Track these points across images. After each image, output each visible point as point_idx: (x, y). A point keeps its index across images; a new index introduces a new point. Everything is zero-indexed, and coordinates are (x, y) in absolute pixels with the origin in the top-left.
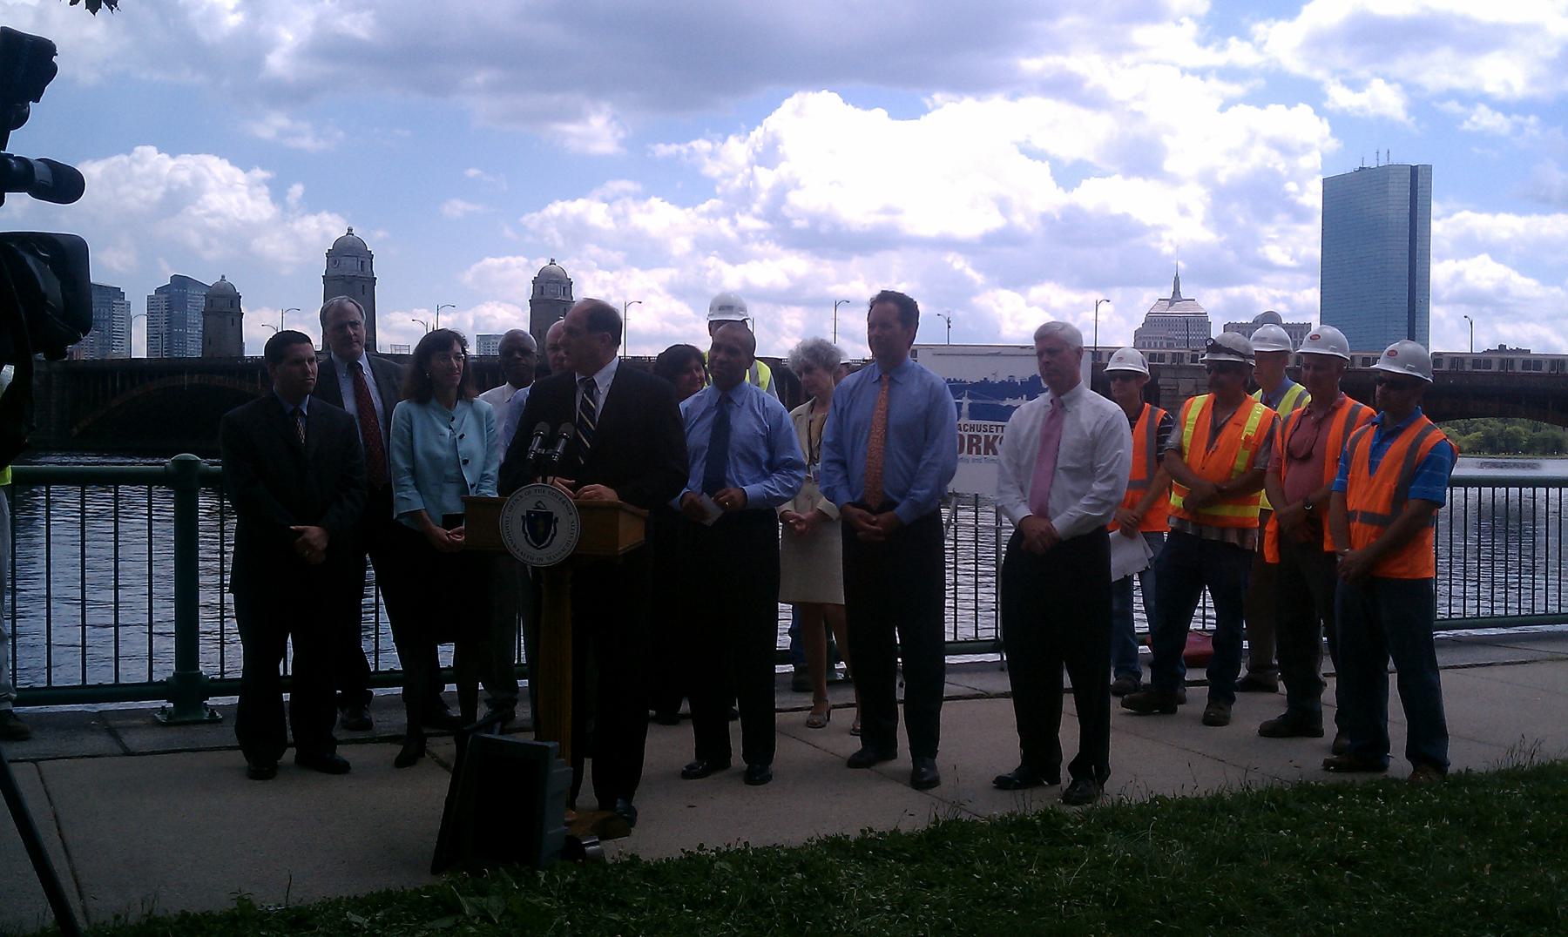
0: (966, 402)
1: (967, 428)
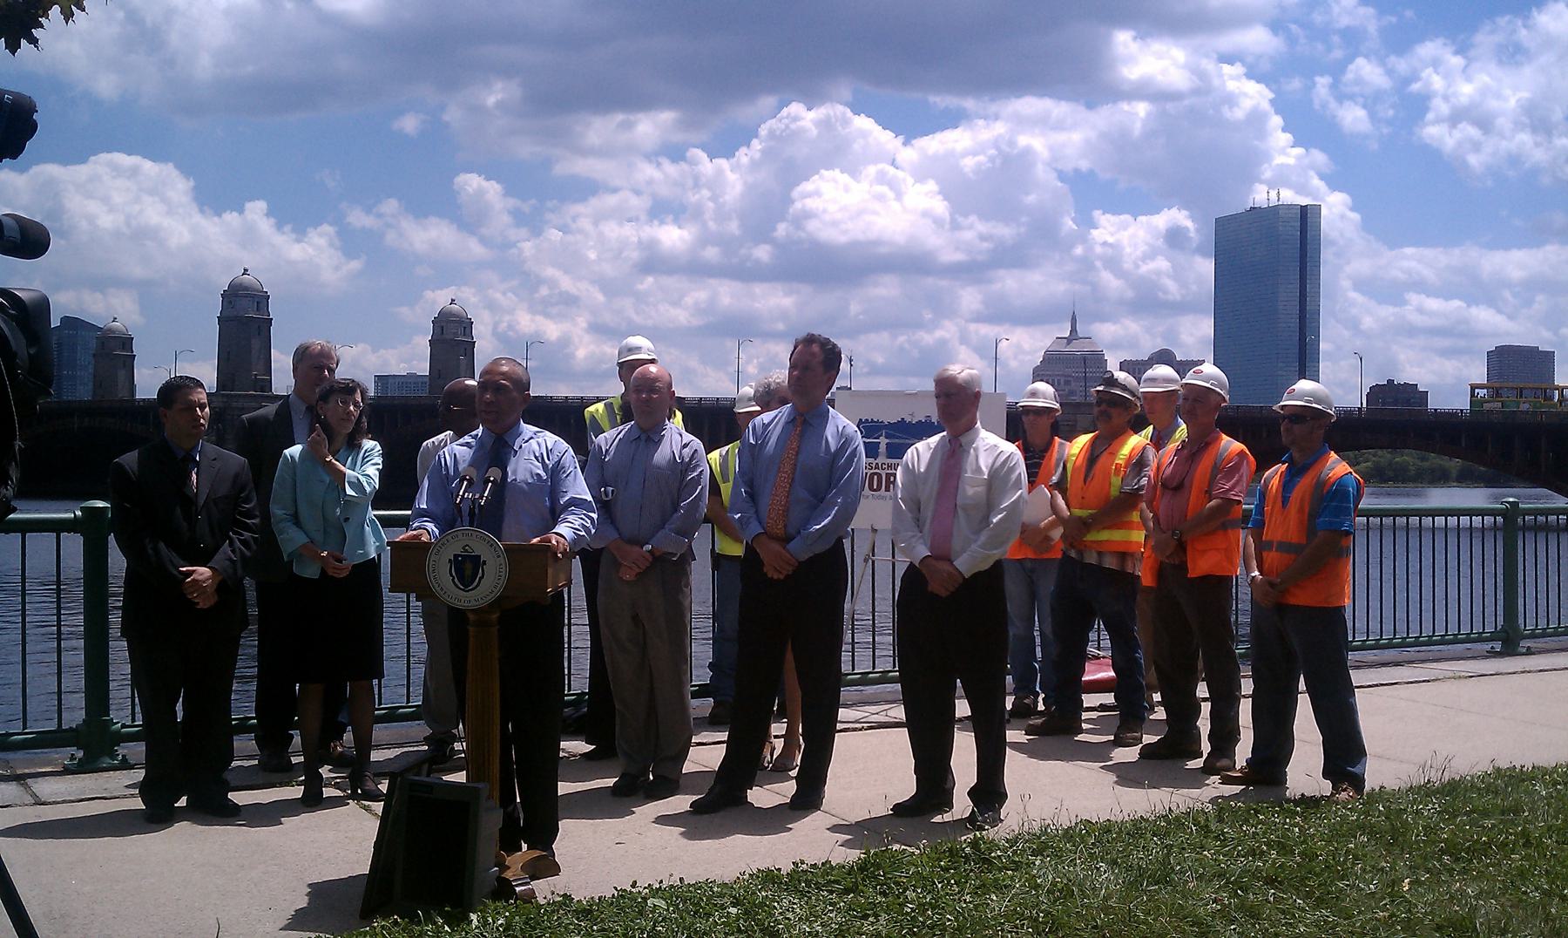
0: (883, 441)
1: (884, 466)
